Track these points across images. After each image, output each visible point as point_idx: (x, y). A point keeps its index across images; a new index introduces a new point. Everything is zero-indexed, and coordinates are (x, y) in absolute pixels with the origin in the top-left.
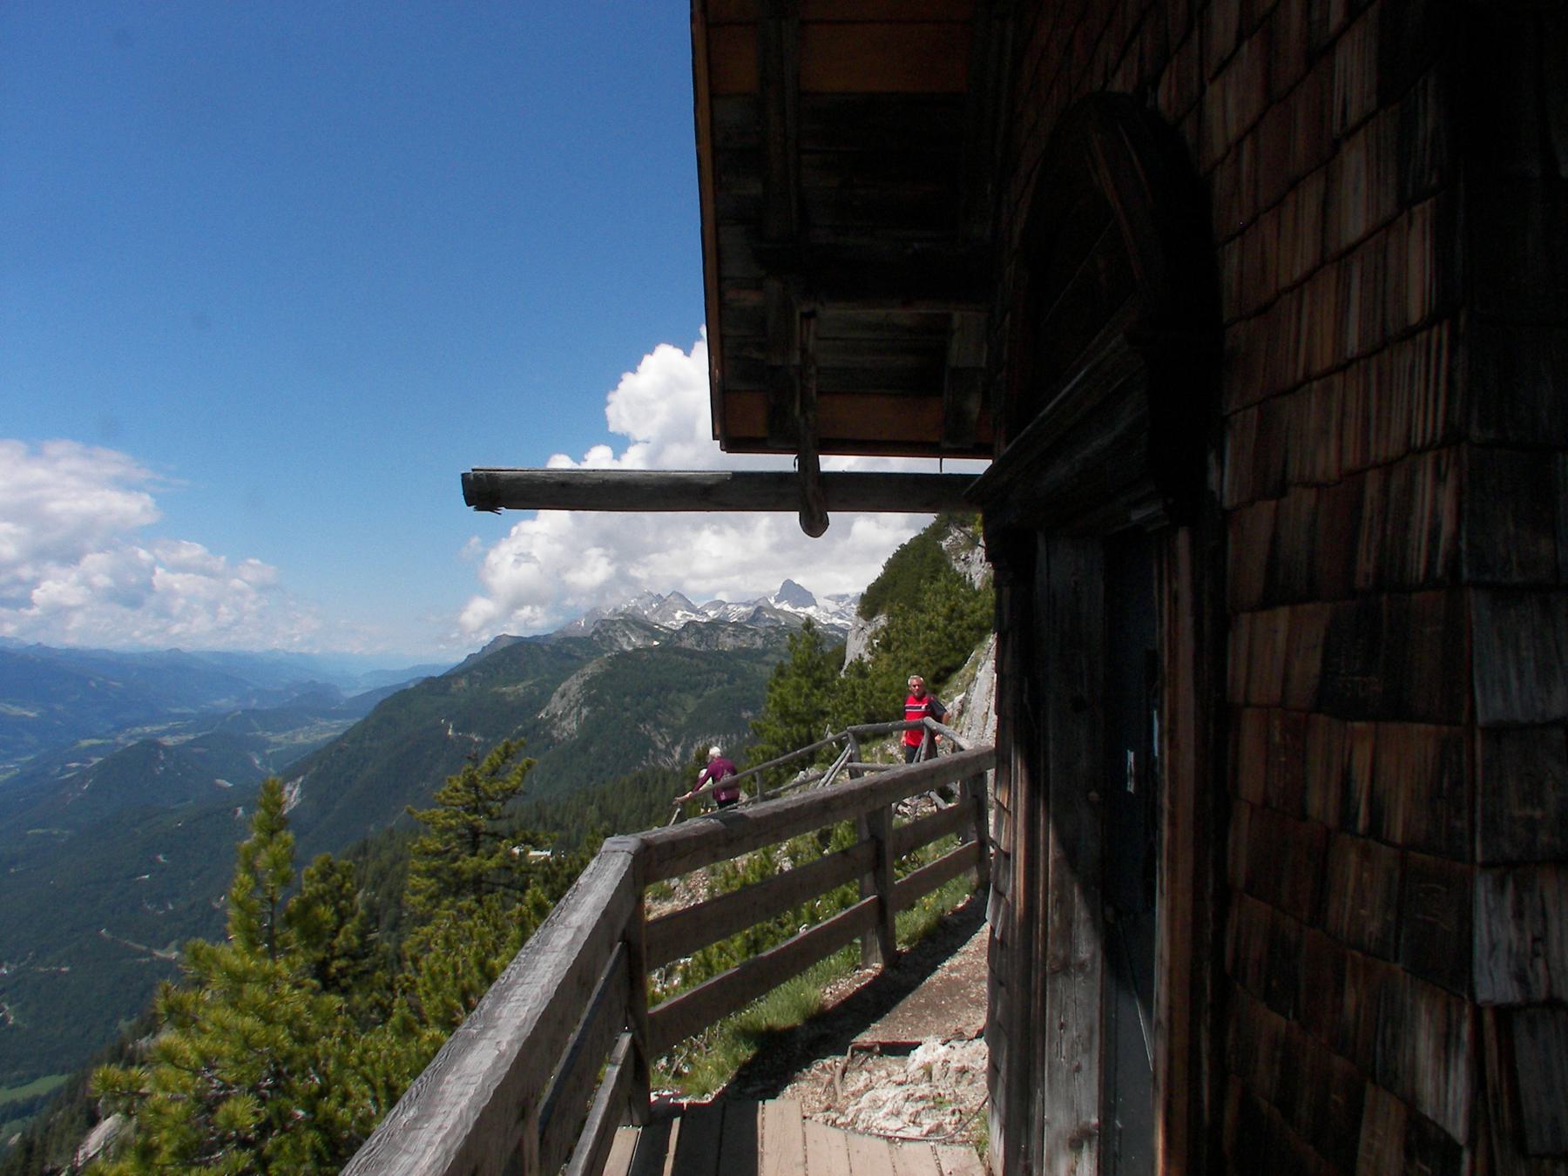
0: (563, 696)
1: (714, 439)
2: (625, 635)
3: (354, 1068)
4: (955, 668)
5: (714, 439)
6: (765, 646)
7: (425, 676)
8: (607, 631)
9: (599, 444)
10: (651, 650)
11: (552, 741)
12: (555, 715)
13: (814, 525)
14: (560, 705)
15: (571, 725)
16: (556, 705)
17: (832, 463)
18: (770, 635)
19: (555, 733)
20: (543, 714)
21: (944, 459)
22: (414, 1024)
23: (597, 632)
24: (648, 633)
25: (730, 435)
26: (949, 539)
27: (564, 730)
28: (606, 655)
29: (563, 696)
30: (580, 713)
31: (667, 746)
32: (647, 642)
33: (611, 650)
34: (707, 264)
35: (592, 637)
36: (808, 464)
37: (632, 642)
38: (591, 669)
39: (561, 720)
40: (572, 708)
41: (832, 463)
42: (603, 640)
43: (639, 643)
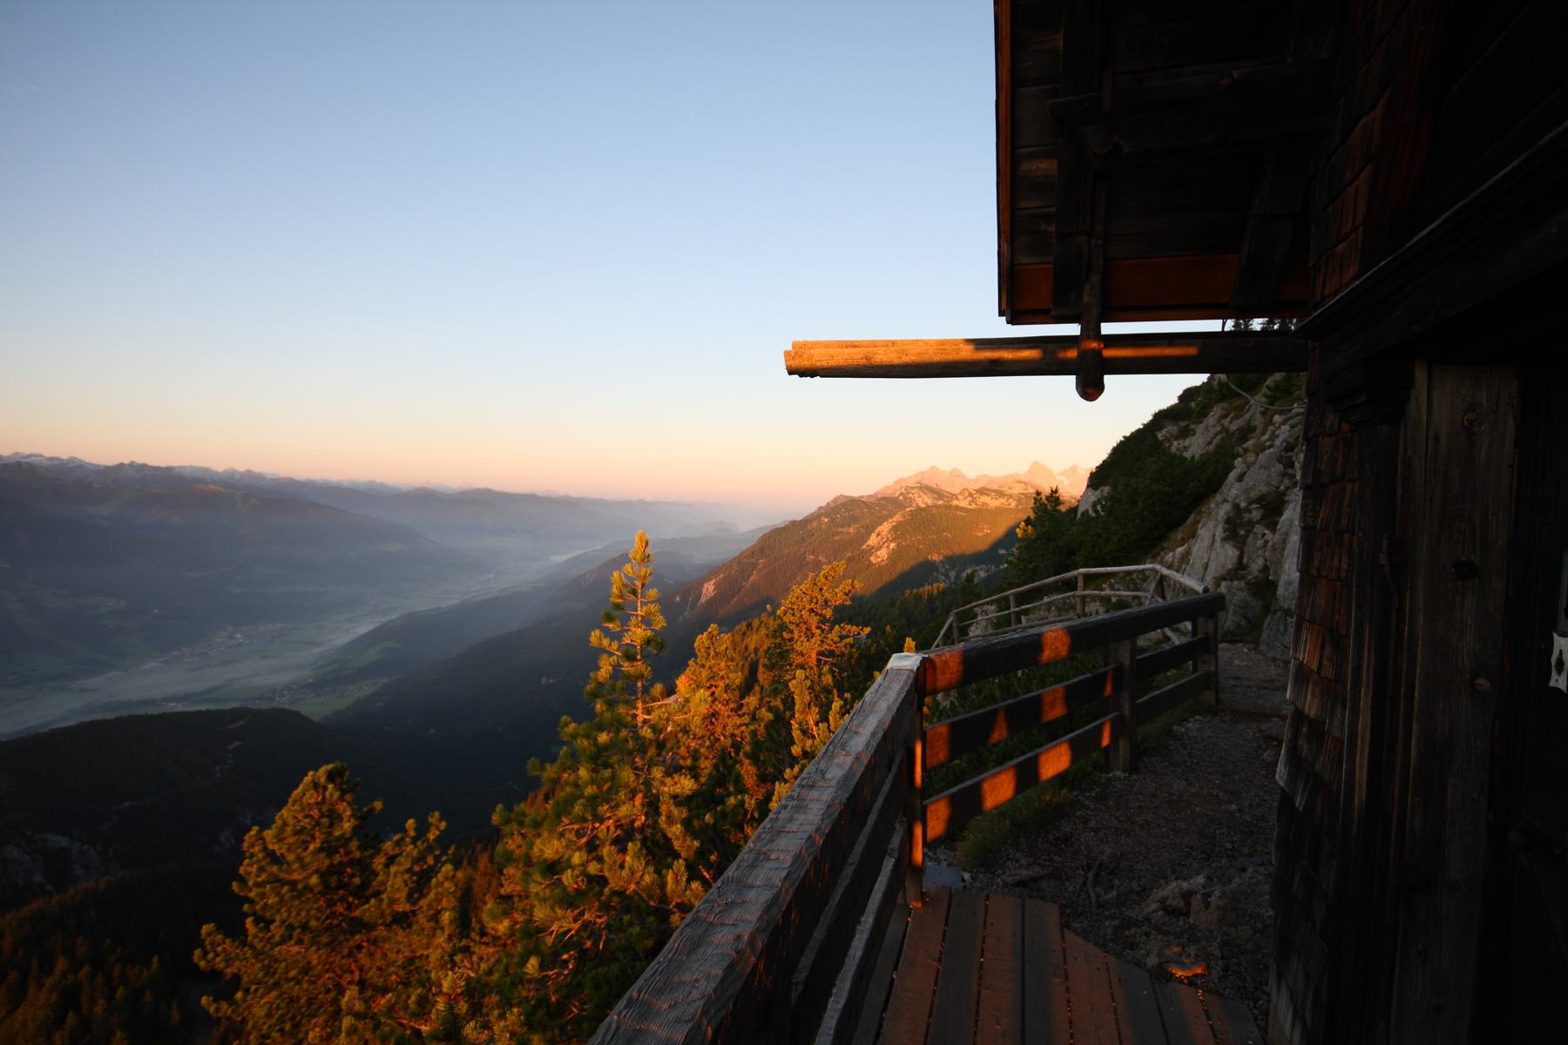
0: (878, 535)
1: (1000, 315)
2: (920, 496)
3: (427, 992)
4: (1179, 522)
5: (1000, 315)
6: (1017, 506)
7: (791, 519)
8: (908, 493)
9: (985, 551)
10: (938, 507)
11: (870, 564)
12: (873, 547)
13: (1090, 389)
14: (875, 541)
15: (883, 554)
16: (873, 540)
17: (1108, 328)
18: (1021, 499)
19: (872, 559)
20: (864, 547)
21: (1220, 330)
22: (703, 780)
23: (902, 494)
24: (935, 496)
25: (1012, 309)
26: (1164, 431)
27: (879, 557)
28: (907, 509)
29: (878, 535)
30: (888, 547)
31: (946, 570)
32: (934, 502)
33: (911, 506)
34: (1001, 217)
35: (898, 497)
36: (1091, 331)
37: (924, 500)
38: (897, 518)
39: (877, 550)
40: (884, 543)
41: (1108, 328)
42: (905, 498)
43: (929, 502)
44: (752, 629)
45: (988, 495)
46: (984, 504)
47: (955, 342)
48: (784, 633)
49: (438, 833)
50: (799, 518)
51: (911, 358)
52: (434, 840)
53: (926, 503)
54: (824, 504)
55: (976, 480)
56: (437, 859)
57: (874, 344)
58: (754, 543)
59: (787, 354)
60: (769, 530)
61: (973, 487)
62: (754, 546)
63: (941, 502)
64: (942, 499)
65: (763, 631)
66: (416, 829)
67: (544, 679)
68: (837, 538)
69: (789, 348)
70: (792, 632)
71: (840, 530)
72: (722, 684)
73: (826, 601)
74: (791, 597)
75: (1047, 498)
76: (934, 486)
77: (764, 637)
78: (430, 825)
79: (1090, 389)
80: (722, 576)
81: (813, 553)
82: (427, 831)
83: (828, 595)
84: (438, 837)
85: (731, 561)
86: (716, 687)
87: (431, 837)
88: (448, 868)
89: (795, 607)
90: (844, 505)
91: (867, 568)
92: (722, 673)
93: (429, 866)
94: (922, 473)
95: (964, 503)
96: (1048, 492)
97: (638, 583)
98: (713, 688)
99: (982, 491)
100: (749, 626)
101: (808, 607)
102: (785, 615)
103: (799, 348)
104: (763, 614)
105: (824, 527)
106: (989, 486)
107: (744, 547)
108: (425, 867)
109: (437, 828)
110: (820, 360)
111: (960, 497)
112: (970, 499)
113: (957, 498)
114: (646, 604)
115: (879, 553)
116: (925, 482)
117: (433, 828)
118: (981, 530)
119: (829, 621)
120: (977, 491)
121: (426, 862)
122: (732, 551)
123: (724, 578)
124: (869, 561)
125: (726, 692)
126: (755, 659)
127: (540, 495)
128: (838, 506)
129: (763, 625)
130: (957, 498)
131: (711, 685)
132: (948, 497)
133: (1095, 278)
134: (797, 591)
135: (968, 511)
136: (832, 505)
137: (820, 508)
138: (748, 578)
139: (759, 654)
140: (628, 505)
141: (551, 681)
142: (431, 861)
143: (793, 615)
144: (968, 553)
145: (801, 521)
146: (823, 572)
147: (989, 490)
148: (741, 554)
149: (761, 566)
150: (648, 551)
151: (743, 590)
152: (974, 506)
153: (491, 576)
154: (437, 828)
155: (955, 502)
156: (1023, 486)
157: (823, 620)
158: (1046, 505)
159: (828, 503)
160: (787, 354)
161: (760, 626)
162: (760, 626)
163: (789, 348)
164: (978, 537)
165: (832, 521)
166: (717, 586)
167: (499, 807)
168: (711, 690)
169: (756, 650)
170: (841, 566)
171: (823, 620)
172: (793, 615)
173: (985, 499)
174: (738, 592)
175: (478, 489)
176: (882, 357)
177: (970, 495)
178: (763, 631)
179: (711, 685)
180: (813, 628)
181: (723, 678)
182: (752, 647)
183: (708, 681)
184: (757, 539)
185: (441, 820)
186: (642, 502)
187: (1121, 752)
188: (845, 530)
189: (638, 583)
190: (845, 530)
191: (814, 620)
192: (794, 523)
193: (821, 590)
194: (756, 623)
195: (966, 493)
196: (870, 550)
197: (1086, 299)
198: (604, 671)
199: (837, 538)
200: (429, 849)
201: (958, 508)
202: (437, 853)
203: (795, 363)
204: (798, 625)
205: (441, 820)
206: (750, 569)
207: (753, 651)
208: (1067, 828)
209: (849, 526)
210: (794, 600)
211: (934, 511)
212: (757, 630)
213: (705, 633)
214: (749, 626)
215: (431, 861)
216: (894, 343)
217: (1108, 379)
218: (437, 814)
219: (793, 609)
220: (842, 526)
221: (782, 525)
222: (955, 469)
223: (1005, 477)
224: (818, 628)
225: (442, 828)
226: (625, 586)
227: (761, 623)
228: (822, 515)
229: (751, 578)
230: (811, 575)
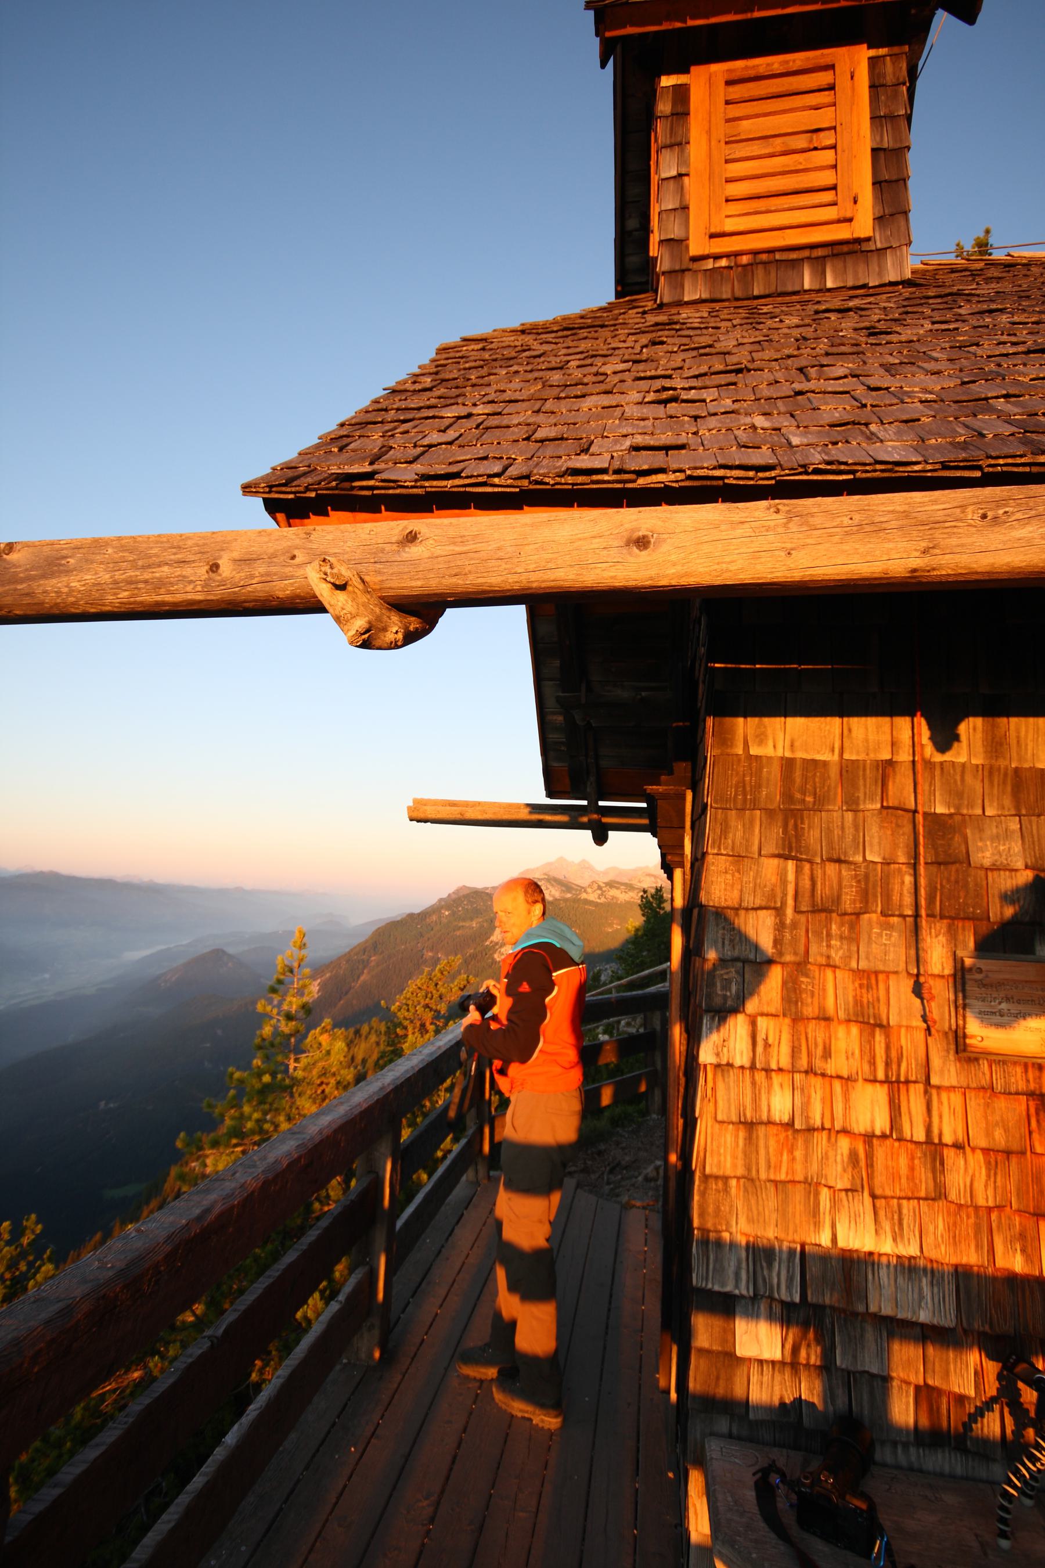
7: (408, 911)
10: (566, 900)
12: (497, 944)
13: (600, 839)
19: (496, 956)
20: (487, 943)
25: (550, 794)
36: (593, 803)
39: (501, 947)
41: (601, 803)
44: (360, 1036)
45: (618, 888)
46: (613, 897)
47: (518, 806)
48: (398, 1030)
49: (33, 1237)
50: (417, 911)
51: (489, 816)
52: (29, 1244)
53: (553, 896)
54: (445, 896)
55: (605, 873)
56: (30, 1265)
57: (466, 804)
58: (367, 937)
59: (409, 808)
60: (383, 924)
61: (602, 880)
62: (367, 941)
63: (569, 895)
64: (570, 892)
65: (373, 1038)
66: (11, 1232)
67: (102, 1104)
68: (458, 933)
69: (411, 804)
70: (405, 1028)
71: (461, 924)
72: (333, 1081)
73: (441, 997)
74: (407, 993)
75: (652, 896)
76: (562, 877)
77: (374, 1046)
78: (26, 1228)
79: (600, 839)
80: (328, 975)
81: (431, 950)
82: (22, 1234)
83: (442, 990)
84: (34, 1240)
85: (339, 958)
86: (327, 1084)
87: (25, 1241)
88: (48, 1268)
89: (410, 1002)
90: (466, 896)
91: (490, 967)
92: (334, 1070)
93: (21, 1273)
94: (550, 864)
95: (593, 897)
96: (653, 891)
97: (296, 965)
98: (324, 1086)
99: (611, 884)
100: (357, 1032)
101: (423, 1003)
102: (399, 1010)
103: (419, 803)
104: (374, 1019)
105: (444, 920)
106: (618, 879)
107: (355, 942)
108: (17, 1273)
109: (33, 1231)
110: (431, 813)
111: (589, 890)
112: (599, 892)
113: (585, 891)
114: (302, 979)
115: (503, 950)
116: (554, 874)
117: (28, 1231)
118: (611, 925)
119: (443, 1017)
120: (607, 884)
121: (18, 1269)
122: (341, 946)
123: (330, 978)
124: (493, 959)
125: (337, 1088)
126: (363, 1071)
127: (118, 880)
128: (459, 898)
129: (373, 1031)
130: (585, 891)
131: (322, 1083)
132: (576, 890)
133: (592, 779)
134: (412, 985)
135: (596, 905)
136: (454, 896)
137: (441, 900)
138: (359, 977)
139: (367, 1065)
140: (222, 893)
141: (112, 1105)
142: (23, 1267)
143: (408, 1010)
144: (597, 950)
145: (419, 914)
146: (438, 967)
147: (618, 883)
148: (352, 950)
149: (373, 964)
150: (305, 940)
151: (352, 991)
152: (603, 900)
153: (47, 976)
154: (33, 1231)
155: (584, 896)
156: (653, 879)
157: (437, 1015)
158: (651, 903)
159: (449, 895)
160: (409, 808)
161: (369, 1033)
162: (369, 1033)
163: (411, 804)
164: (608, 933)
165: (453, 914)
166: (323, 987)
167: (182, 1135)
168: (321, 1088)
169: (364, 1061)
170: (458, 960)
171: (437, 1015)
172: (408, 1010)
173: (614, 892)
174: (347, 993)
175: (42, 873)
176: (471, 815)
177: (600, 888)
178: (373, 1038)
179: (322, 1083)
180: (428, 1024)
181: (334, 1075)
182: (359, 1058)
183: (319, 1077)
184: (370, 933)
185: (37, 1223)
186: (239, 890)
187: (656, 1099)
188: (467, 924)
189: (296, 965)
190: (467, 924)
191: (428, 1016)
192: (411, 916)
193: (436, 985)
194: (365, 1029)
195: (595, 886)
196: (493, 946)
197: (588, 790)
198: (267, 1030)
199: (458, 933)
200: (22, 1255)
201: (587, 902)
202: (31, 1258)
203: (415, 815)
204: (412, 1022)
205: (37, 1223)
206: (361, 967)
207: (360, 1062)
208: (602, 1147)
209: (472, 919)
210: (409, 995)
211: (562, 905)
212: (366, 1037)
213: (319, 1029)
214: (357, 1032)
215: (23, 1267)
216: (479, 803)
217: (610, 833)
218: (33, 1216)
219: (408, 1005)
220: (464, 920)
221: (399, 919)
222: (584, 861)
223: (635, 870)
224: (431, 1024)
225: (38, 1232)
226: (286, 966)
227: (371, 1028)
228: (442, 907)
229: (362, 978)
230: (427, 969)
